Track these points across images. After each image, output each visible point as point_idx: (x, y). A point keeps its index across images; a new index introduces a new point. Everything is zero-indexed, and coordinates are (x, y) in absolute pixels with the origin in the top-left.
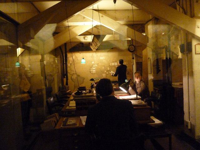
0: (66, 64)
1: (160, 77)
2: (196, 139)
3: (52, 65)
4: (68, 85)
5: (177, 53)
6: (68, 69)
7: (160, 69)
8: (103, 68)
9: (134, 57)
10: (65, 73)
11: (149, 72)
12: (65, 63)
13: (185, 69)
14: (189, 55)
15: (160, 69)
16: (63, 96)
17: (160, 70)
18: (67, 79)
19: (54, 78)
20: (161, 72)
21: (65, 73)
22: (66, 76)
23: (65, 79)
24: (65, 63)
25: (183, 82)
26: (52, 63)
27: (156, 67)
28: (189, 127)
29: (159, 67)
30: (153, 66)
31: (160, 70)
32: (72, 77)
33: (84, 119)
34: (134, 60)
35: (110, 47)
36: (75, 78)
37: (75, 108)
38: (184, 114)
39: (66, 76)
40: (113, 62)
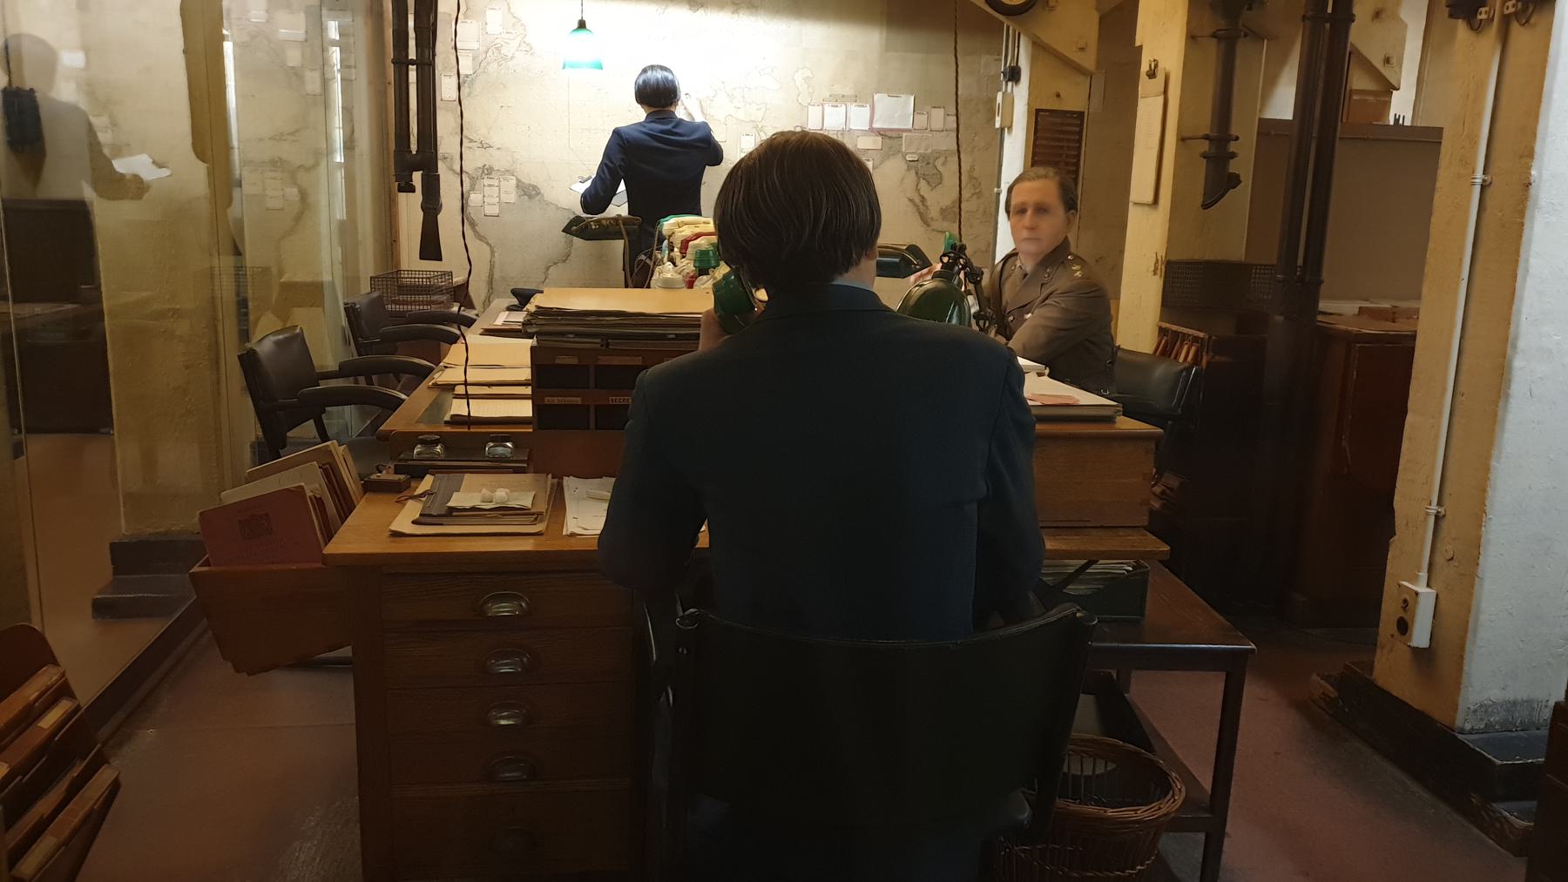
0: (427, 67)
1: (1232, 235)
2: (1462, 732)
3: (296, 74)
4: (437, 256)
5: (1387, 61)
6: (445, 124)
7: (1233, 167)
9: (1024, 64)
10: (414, 147)
11: (1133, 197)
12: (412, 55)
13: (1469, 165)
14: (1520, 36)
15: (1231, 170)
16: (406, 327)
17: (1235, 181)
18: (431, 205)
19: (304, 196)
20: (1240, 199)
21: (414, 147)
22: (417, 177)
23: (410, 207)
24: (412, 55)
25: (1418, 297)
26: (294, 57)
27: (1205, 146)
28: (1420, 636)
29: (1233, 147)
30: (1182, 140)
31: (1235, 181)
32: (474, 199)
33: (586, 516)
34: (1021, 94)
36: (495, 210)
37: (524, 409)
38: (1391, 531)
39: (417, 177)
40: (837, 99)
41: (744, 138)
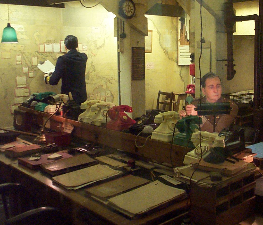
8: (19, 58)
35: (128, 4)
41: (17, 57)
